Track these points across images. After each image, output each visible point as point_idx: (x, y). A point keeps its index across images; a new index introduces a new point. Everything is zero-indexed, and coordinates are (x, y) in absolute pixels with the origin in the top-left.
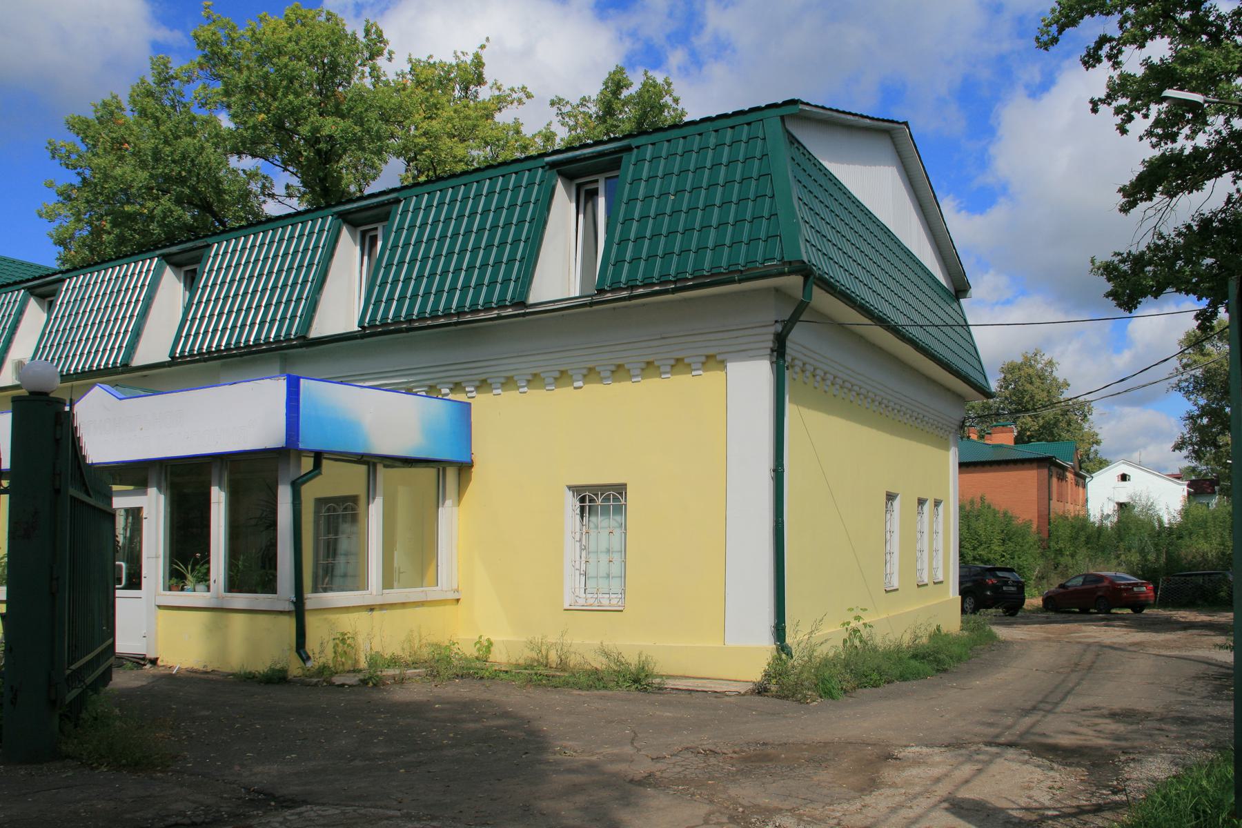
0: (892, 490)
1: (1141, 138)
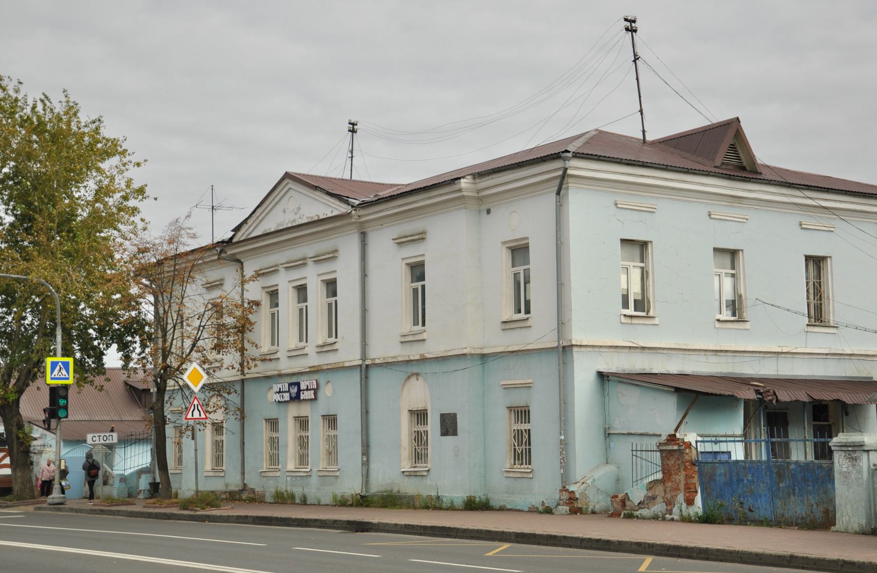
0: (462, 424)
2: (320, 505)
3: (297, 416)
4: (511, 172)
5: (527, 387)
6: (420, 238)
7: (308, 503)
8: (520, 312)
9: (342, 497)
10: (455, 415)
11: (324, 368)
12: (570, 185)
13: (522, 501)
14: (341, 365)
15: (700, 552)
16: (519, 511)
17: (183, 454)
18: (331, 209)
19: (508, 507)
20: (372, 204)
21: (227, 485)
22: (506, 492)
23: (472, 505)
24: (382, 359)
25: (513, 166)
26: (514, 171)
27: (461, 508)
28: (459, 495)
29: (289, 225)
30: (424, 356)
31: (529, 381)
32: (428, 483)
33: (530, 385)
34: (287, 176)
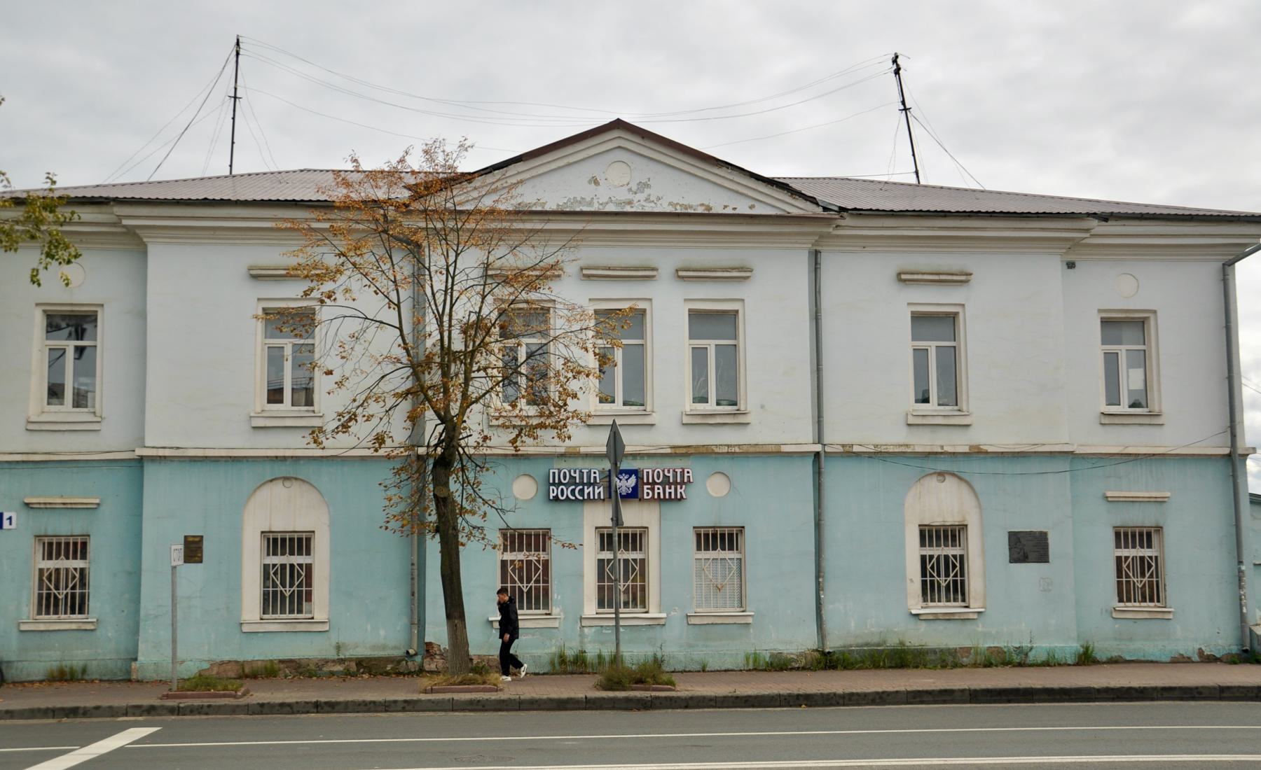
0: (178, 548)
1: (578, 399)
2: (130, 680)
3: (267, 530)
4: (1164, 223)
5: (1160, 502)
6: (961, 279)
7: (707, 669)
8: (704, 400)
9: (772, 656)
10: (1009, 532)
11: (717, 450)
12: (20, 244)
13: (1152, 649)
14: (774, 449)
15: (746, 701)
16: (1152, 662)
17: (37, 592)
18: (751, 202)
19: (1128, 658)
20: (935, 216)
21: (338, 648)
22: (1115, 639)
23: (1086, 659)
24: (873, 447)
25: (936, 214)
26: (1169, 223)
27: (1069, 662)
28: (1068, 646)
29: (611, 208)
30: (979, 448)
31: (1168, 494)
32: (980, 629)
33: (1166, 500)
34: (618, 125)
